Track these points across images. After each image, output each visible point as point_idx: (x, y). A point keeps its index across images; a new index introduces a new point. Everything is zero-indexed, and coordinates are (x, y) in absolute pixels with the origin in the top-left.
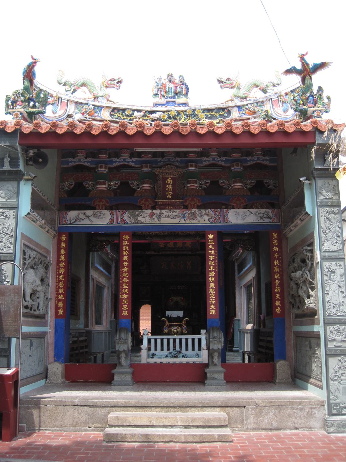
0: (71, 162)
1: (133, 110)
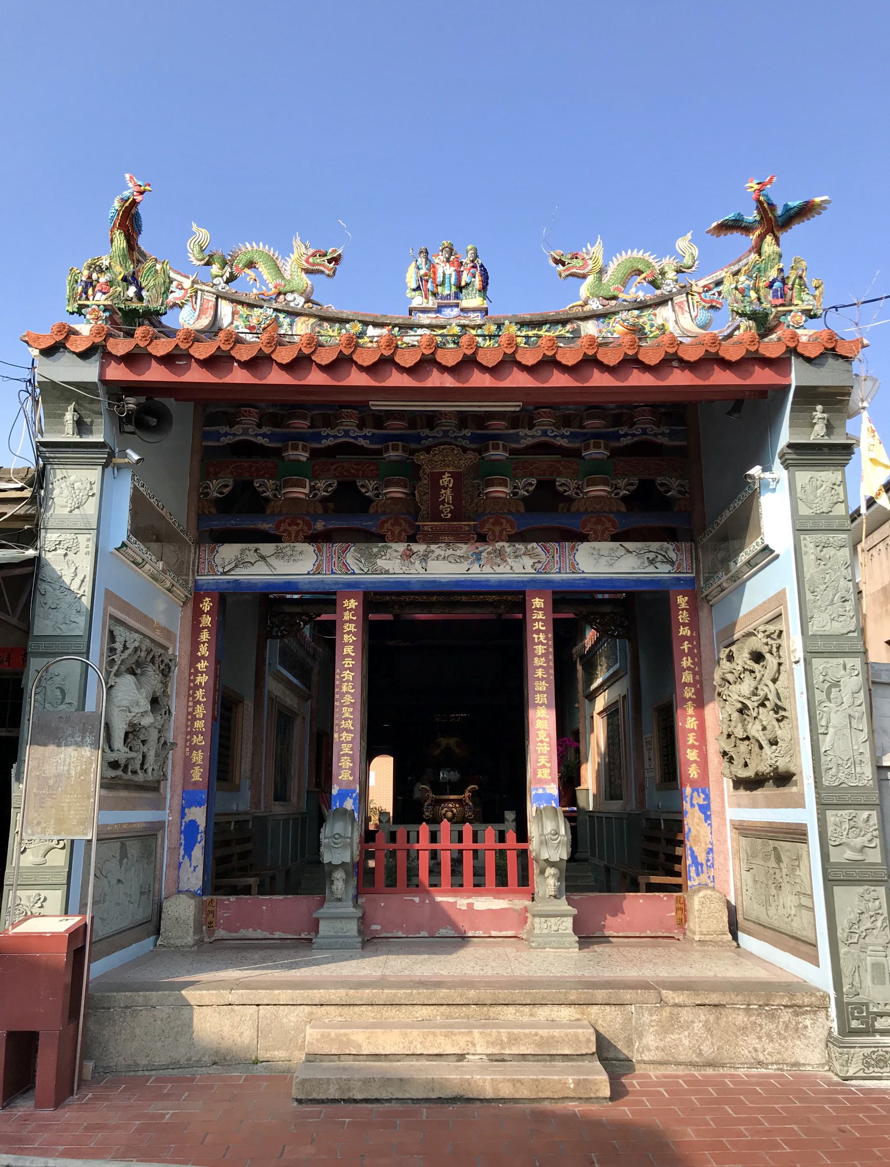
0: (226, 434)
1: (366, 324)
